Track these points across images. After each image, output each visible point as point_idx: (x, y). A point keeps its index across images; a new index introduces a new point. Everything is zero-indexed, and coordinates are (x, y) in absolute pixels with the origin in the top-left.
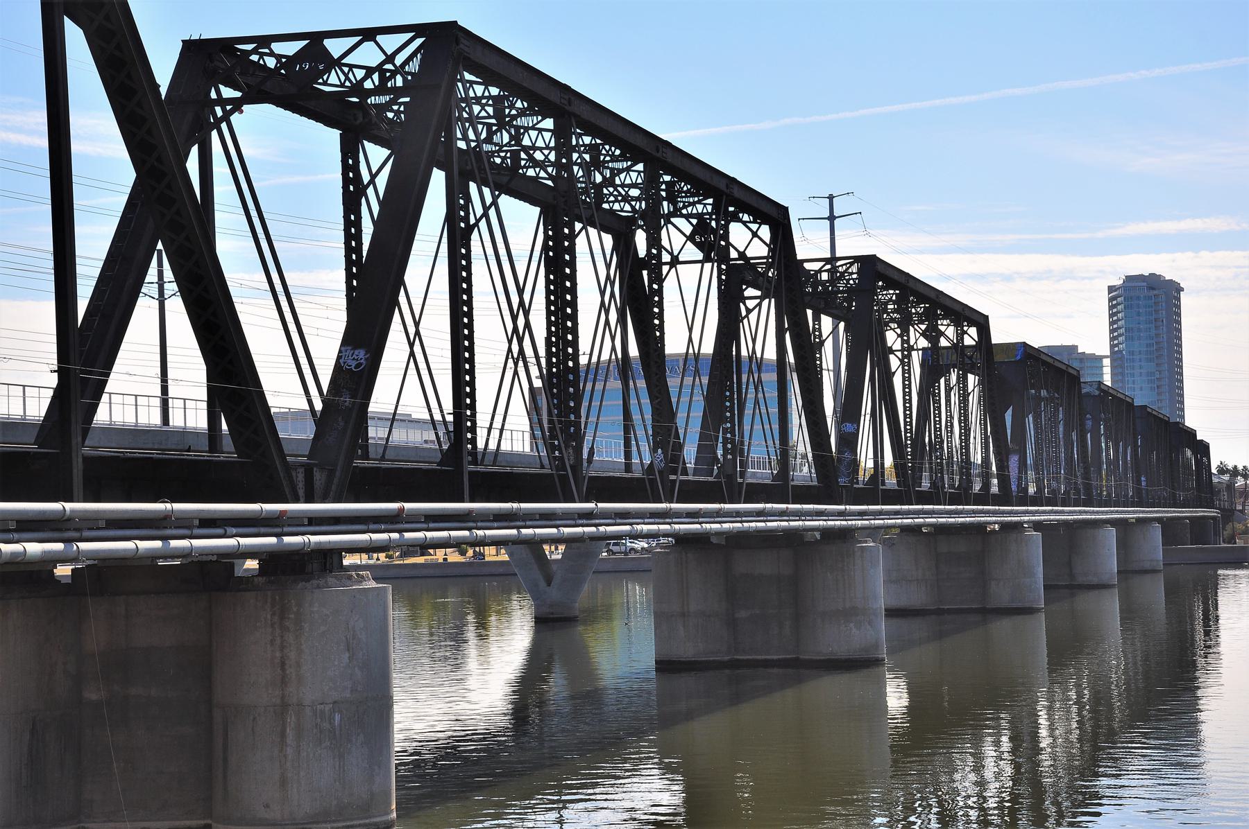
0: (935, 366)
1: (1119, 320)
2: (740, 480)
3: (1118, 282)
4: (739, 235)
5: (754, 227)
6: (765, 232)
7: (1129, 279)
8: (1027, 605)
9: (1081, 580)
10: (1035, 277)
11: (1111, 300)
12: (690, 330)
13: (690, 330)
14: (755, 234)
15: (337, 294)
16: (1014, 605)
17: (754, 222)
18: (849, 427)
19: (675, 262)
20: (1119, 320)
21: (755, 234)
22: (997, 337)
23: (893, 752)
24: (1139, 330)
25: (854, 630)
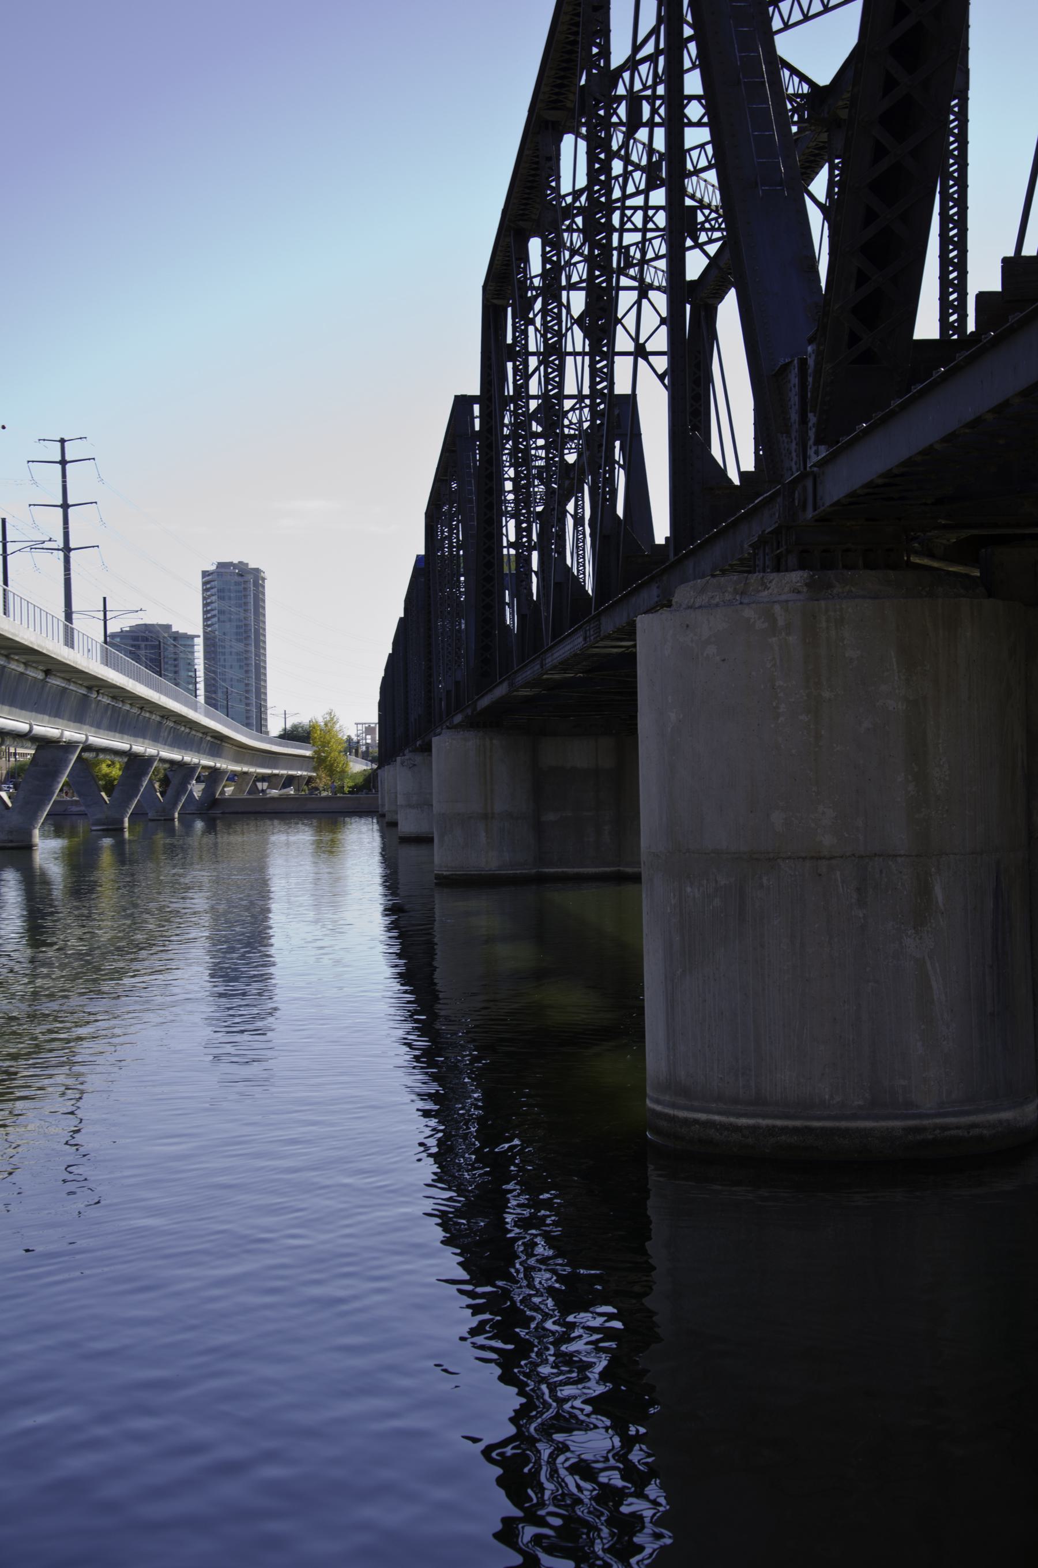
7: (221, 565)
20: (212, 603)
24: (230, 612)
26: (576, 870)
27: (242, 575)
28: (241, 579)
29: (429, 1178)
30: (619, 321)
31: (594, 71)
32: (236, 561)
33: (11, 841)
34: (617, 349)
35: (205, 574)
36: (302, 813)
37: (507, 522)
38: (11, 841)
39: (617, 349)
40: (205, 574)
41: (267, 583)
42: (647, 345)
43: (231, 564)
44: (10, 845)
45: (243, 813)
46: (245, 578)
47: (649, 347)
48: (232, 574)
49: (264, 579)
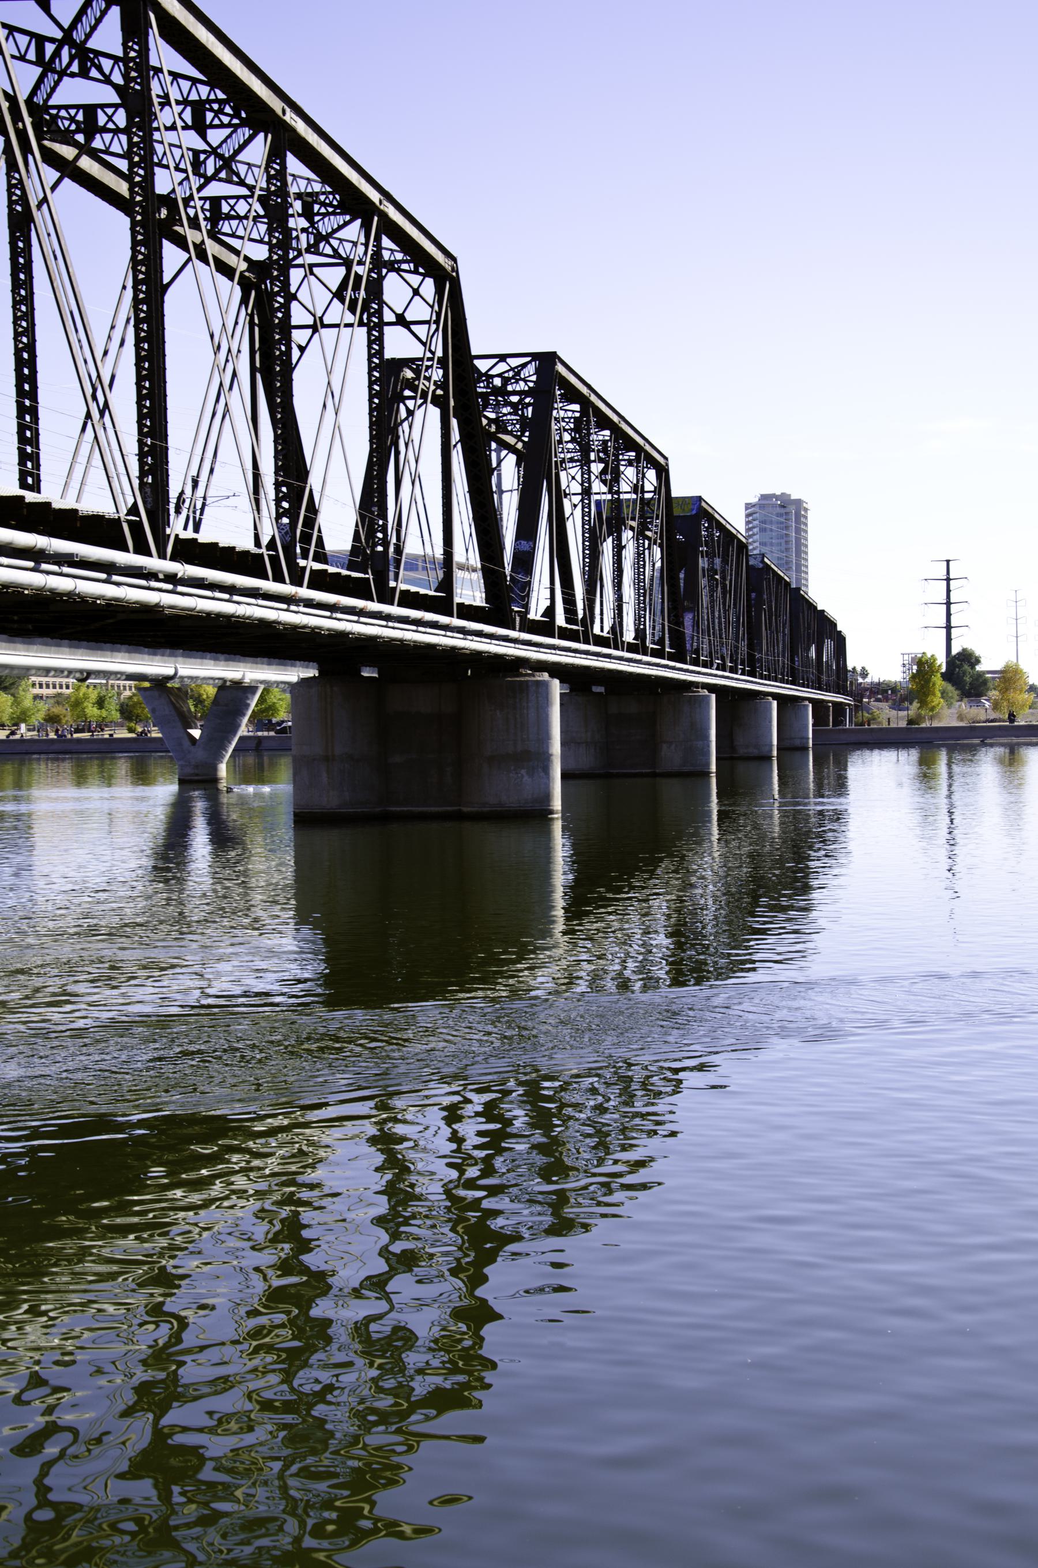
0: (608, 522)
1: (754, 535)
2: (392, 584)
3: (754, 500)
4: (396, 290)
5: (415, 280)
6: (428, 288)
7: (764, 497)
8: (698, 769)
9: (742, 752)
10: (601, 597)
11: (747, 516)
12: (329, 373)
13: (329, 373)
14: (416, 292)
15: (72, 493)
16: (686, 769)
17: (416, 272)
18: (525, 546)
19: (317, 326)
20: (754, 535)
21: (416, 292)
22: (679, 489)
23: (684, 984)
24: (772, 544)
25: (526, 778)
26: (420, 809)
27: (784, 507)
28: (783, 511)
29: (379, 1188)
30: (294, 297)
31: (137, 120)
32: (778, 493)
33: (197, 775)
34: (293, 323)
35: (748, 506)
36: (855, 744)
37: (499, 462)
38: (197, 775)
39: (293, 323)
40: (748, 506)
41: (810, 514)
42: (406, 315)
43: (774, 496)
44: (196, 778)
45: (855, 744)
46: (787, 510)
47: (409, 317)
48: (774, 506)
49: (806, 510)
